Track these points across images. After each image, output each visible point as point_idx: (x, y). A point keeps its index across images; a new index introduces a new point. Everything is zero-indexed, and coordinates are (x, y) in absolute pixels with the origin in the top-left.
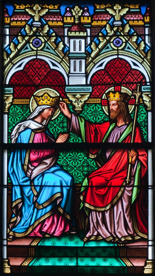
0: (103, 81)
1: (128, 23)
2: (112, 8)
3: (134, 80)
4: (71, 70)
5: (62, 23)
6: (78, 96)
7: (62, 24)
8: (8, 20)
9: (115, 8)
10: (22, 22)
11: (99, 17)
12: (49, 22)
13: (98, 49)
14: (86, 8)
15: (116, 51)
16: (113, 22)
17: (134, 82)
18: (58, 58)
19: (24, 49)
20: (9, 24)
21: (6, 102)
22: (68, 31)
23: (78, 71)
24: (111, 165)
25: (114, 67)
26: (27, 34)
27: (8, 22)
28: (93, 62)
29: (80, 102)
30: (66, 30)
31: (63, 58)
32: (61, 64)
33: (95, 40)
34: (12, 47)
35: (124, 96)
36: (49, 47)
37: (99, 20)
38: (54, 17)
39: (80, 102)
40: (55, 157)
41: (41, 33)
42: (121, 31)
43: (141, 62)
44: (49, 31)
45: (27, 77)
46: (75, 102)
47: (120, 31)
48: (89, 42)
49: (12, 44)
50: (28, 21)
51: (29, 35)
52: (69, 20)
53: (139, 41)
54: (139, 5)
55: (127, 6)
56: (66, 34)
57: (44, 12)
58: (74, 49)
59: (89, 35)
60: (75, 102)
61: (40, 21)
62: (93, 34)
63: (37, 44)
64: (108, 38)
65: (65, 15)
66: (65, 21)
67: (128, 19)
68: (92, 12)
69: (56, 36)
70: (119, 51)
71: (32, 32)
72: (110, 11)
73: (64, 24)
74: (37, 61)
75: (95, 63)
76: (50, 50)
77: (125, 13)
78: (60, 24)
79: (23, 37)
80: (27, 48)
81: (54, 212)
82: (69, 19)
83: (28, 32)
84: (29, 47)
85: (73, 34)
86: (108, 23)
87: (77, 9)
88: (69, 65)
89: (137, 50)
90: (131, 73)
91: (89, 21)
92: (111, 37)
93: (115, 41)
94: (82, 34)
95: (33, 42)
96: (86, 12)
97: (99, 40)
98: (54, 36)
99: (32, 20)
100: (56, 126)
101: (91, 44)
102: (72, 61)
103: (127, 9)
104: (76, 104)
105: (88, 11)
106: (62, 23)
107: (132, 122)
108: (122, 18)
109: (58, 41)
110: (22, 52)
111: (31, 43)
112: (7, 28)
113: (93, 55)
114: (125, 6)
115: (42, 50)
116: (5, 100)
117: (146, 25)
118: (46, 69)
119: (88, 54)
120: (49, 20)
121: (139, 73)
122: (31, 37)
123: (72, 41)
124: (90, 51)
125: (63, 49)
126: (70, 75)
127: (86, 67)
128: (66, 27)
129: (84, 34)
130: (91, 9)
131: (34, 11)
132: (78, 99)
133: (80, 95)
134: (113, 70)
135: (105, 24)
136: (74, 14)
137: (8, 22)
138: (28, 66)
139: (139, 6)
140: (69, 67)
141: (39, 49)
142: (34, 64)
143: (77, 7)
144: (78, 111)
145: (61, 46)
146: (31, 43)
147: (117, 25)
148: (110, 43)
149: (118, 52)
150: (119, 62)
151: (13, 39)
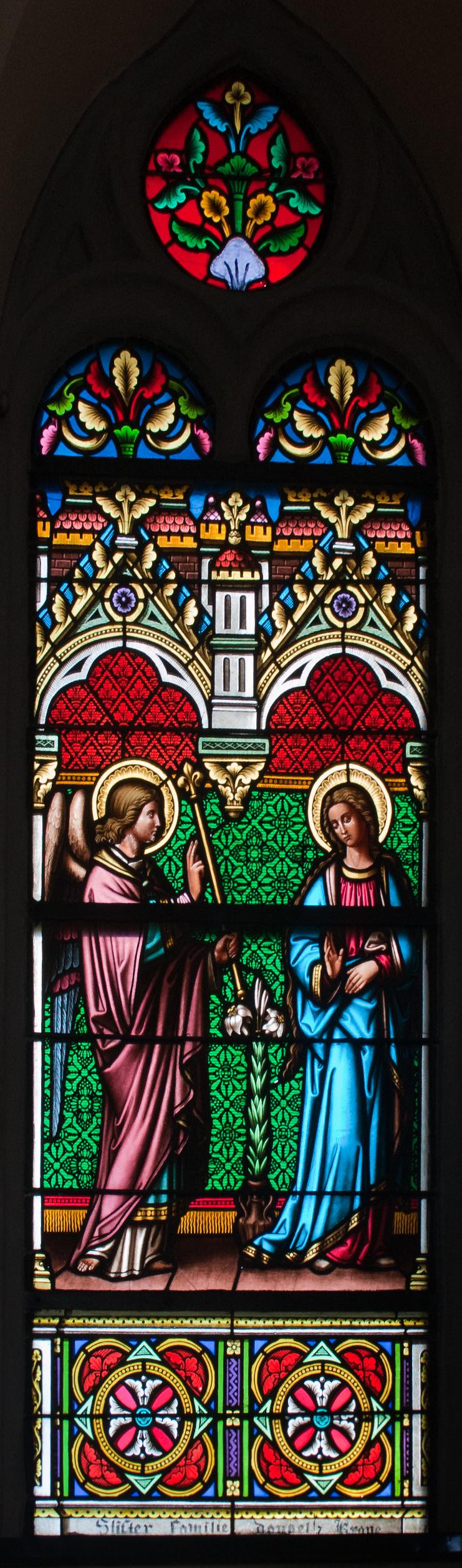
0: (81, 718)
1: (372, 548)
2: (110, 496)
3: (386, 723)
4: (216, 687)
6: (234, 767)
7: (195, 545)
8: (44, 529)
9: (119, 497)
10: (171, 538)
12: (159, 538)
13: (290, 625)
14: (258, 503)
15: (120, 627)
16: (333, 543)
17: (386, 728)
18: (402, 657)
19: (308, 625)
22: (212, 567)
23: (234, 690)
25: (332, 682)
26: (319, 576)
28: (56, 658)
29: (238, 786)
30: (206, 562)
31: (196, 648)
32: (190, 667)
33: (282, 597)
34: (57, 608)
36: (378, 623)
37: (292, 537)
38: (304, 525)
39: (238, 786)
41: (135, 570)
42: (135, 565)
43: (185, 662)
45: (286, 708)
46: (225, 785)
47: (131, 565)
49: (277, 605)
50: (321, 538)
52: (215, 533)
53: (182, 598)
54: (401, 495)
55: (368, 497)
56: (205, 576)
57: (143, 509)
58: (227, 624)
59: (266, 577)
60: (225, 785)
61: (352, 538)
62: (56, 571)
63: (346, 607)
64: (96, 586)
65: (205, 518)
68: (274, 515)
69: (179, 580)
70: (128, 627)
72: (108, 508)
73: (201, 543)
74: (344, 660)
75: (63, 660)
76: (380, 629)
77: (363, 517)
78: (189, 543)
79: (308, 586)
83: (319, 571)
84: (101, 613)
85: (224, 575)
86: (316, 546)
87: (126, 496)
88: (210, 672)
89: (396, 632)
90: (380, 701)
91: (268, 538)
92: (105, 583)
94: (247, 576)
95: (112, 596)
96: (212, 511)
97: (293, 595)
98: (171, 582)
99: (330, 534)
100: (172, 854)
103: (152, 502)
104: (228, 791)
105: (264, 510)
106: (194, 541)
108: (137, 526)
109: (402, 605)
110: (305, 632)
111: (327, 606)
112: (43, 552)
113: (275, 643)
115: (357, 629)
116: (36, 772)
117: (202, 549)
118: (117, 682)
119: (263, 636)
121: (182, 698)
123: (220, 596)
124: (268, 627)
125: (199, 619)
126: (214, 701)
129: (253, 576)
130: (273, 506)
132: (233, 776)
133: (239, 763)
134: (363, 690)
135: (89, 544)
136: (227, 517)
138: (318, 674)
139: (401, 500)
140: (212, 679)
142: (335, 670)
143: (235, 499)
144: (236, 811)
145: (192, 612)
146: (327, 606)
147: (342, 553)
148: (324, 606)
149: (343, 637)
150: (347, 664)
151: (280, 593)
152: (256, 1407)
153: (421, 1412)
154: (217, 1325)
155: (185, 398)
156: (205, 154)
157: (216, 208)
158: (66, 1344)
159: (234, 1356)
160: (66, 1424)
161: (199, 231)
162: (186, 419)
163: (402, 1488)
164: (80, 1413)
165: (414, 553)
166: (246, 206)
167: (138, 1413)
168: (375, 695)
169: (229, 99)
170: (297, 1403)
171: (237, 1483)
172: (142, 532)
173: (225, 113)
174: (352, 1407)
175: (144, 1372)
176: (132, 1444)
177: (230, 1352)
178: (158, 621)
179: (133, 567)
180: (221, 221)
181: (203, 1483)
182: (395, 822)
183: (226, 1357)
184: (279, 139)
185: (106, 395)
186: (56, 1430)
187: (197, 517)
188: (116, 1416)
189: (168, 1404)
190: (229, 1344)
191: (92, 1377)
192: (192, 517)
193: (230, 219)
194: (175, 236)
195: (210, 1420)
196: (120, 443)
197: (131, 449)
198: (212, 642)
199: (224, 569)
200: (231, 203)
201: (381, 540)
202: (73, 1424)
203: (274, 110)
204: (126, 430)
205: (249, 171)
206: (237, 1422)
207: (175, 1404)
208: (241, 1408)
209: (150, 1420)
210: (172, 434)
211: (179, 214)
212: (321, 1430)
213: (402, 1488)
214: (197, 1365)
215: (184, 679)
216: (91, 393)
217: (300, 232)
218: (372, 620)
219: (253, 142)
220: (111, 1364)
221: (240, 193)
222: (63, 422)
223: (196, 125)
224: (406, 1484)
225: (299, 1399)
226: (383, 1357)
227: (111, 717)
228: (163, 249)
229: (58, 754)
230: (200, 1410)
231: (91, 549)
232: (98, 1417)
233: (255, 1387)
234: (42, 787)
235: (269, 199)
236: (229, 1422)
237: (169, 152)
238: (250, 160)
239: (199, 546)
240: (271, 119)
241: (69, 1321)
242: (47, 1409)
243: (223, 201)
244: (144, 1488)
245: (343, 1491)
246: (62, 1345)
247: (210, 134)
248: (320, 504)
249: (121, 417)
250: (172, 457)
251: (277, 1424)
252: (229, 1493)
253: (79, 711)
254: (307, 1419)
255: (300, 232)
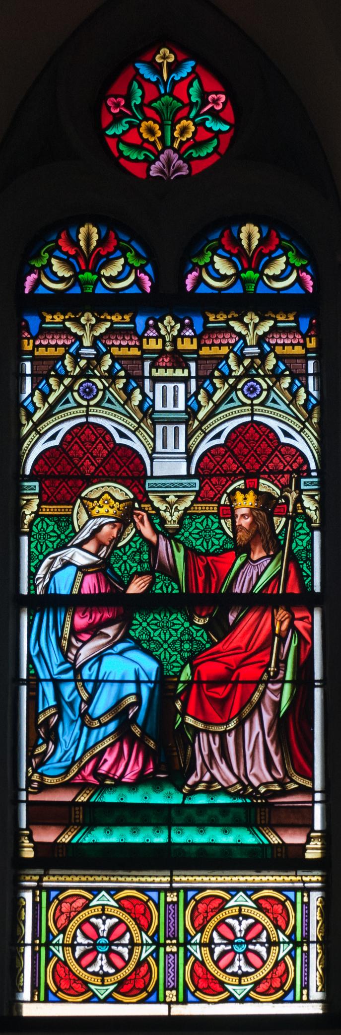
0: (222, 468)
1: (273, 350)
2: (240, 320)
3: (285, 466)
4: (157, 445)
5: (139, 351)
6: (172, 498)
7: (139, 353)
9: (246, 320)
11: (213, 339)
13: (211, 404)
14: (187, 321)
15: (249, 408)
17: (285, 470)
18: (132, 422)
20: (31, 353)
21: (24, 510)
22: (151, 367)
23: (171, 448)
24: (238, 639)
26: (68, 372)
27: (30, 348)
28: (202, 431)
30: (147, 364)
31: (141, 421)
32: (137, 433)
33: (205, 385)
35: (265, 499)
36: (113, 400)
37: (213, 345)
40: (125, 622)
41: (96, 371)
42: (259, 367)
43: (299, 430)
44: (112, 367)
46: (165, 511)
47: (256, 367)
48: (193, 389)
49: (37, 392)
50: (234, 345)
51: (72, 374)
52: (153, 345)
53: (295, 388)
54: (294, 313)
55: (270, 316)
56: (147, 374)
57: (102, 329)
58: (164, 403)
59: (193, 374)
60: (165, 511)
61: (94, 346)
62: (201, 373)
63: (88, 393)
64: (231, 381)
65: (146, 335)
66: (145, 347)
67: (273, 342)
68: (199, 329)
69: (128, 376)
70: (255, 407)
71: (78, 370)
72: (237, 327)
73: (144, 352)
75: (207, 431)
77: (267, 329)
78: (135, 352)
79: (60, 378)
80: (67, 401)
81: (123, 733)
82: (152, 342)
83: (69, 369)
84: (71, 400)
85: (161, 373)
86: (231, 351)
88: (152, 436)
89: (291, 406)
90: (280, 452)
91: (194, 346)
92: (239, 379)
93: (246, 386)
94: (179, 373)
97: (214, 385)
98: (122, 377)
99: (77, 343)
101: (197, 393)
102: (159, 428)
103: (271, 323)
105: (191, 326)
106: (139, 351)
107: (67, 293)
108: (261, 340)
109: (131, 387)
112: (27, 360)
113: (201, 415)
114: (266, 315)
115: (98, 405)
116: (23, 507)
119: (191, 412)
120: (113, 345)
121: (296, 453)
122: (75, 379)
123: (159, 387)
124: (195, 407)
125: (142, 403)
126: (154, 455)
127: (188, 440)
128: (147, 359)
130: (198, 322)
131: (83, 327)
132: (171, 505)
133: (176, 496)
134: (244, 445)
136: (163, 332)
137: (30, 348)
138: (69, 438)
139: (295, 317)
140: (154, 440)
141: (92, 403)
145: (137, 397)
148: (237, 390)
149: (252, 410)
151: (39, 384)
152: (189, 938)
153: (318, 942)
154: (160, 880)
155: (293, 252)
156: (142, 97)
157: (151, 131)
158: (44, 894)
159: (172, 902)
160: (43, 950)
161: (138, 148)
162: (293, 267)
163: (302, 994)
164: (54, 942)
165: (304, 353)
166: (173, 130)
167: (98, 942)
168: (278, 447)
169: (158, 60)
170: (222, 936)
171: (174, 992)
172: (100, 345)
173: (157, 69)
174: (263, 938)
175: (240, 914)
176: (232, 963)
177: (169, 899)
178: (278, 404)
179: (258, 369)
180: (155, 140)
181: (284, 991)
182: (294, 532)
183: (166, 903)
184: (196, 84)
185: (236, 251)
186: (35, 955)
187: (304, 332)
188: (219, 944)
189: (122, 936)
190: (168, 894)
191: (64, 917)
192: (136, 334)
193: (162, 139)
194: (121, 152)
195: (154, 947)
196: (245, 282)
197: (253, 287)
198: (153, 416)
199: (162, 367)
200: (162, 129)
201: (280, 345)
202: (48, 950)
203: (192, 63)
204: (250, 274)
205: (158, 106)
206: (174, 949)
207: (128, 936)
208: (177, 939)
209: (244, 946)
210: (282, 277)
211: (123, 138)
212: (239, 953)
213: (302, 994)
214: (282, 910)
215: (132, 440)
216: (225, 251)
217: (215, 143)
218: (273, 398)
219: (177, 86)
220: (78, 907)
221: (169, 120)
222: (204, 270)
223: (134, 79)
224: (305, 992)
225: (223, 933)
226: (288, 904)
227: (244, 468)
228: (115, 161)
229: (39, 495)
230: (146, 941)
231: (226, 357)
232: (138, 945)
233: (51, 924)
234: (28, 517)
235: (190, 123)
236: (168, 949)
237: (116, 97)
238: (175, 98)
239: (142, 354)
240: (190, 70)
241: (45, 879)
242: (28, 939)
243: (157, 127)
244: (102, 995)
245: (116, 997)
246: (40, 896)
247: (145, 85)
248: (233, 322)
249: (246, 266)
250: (281, 292)
251: (205, 950)
252: (168, 1000)
253: (220, 463)
254: (229, 947)
255: (215, 143)
